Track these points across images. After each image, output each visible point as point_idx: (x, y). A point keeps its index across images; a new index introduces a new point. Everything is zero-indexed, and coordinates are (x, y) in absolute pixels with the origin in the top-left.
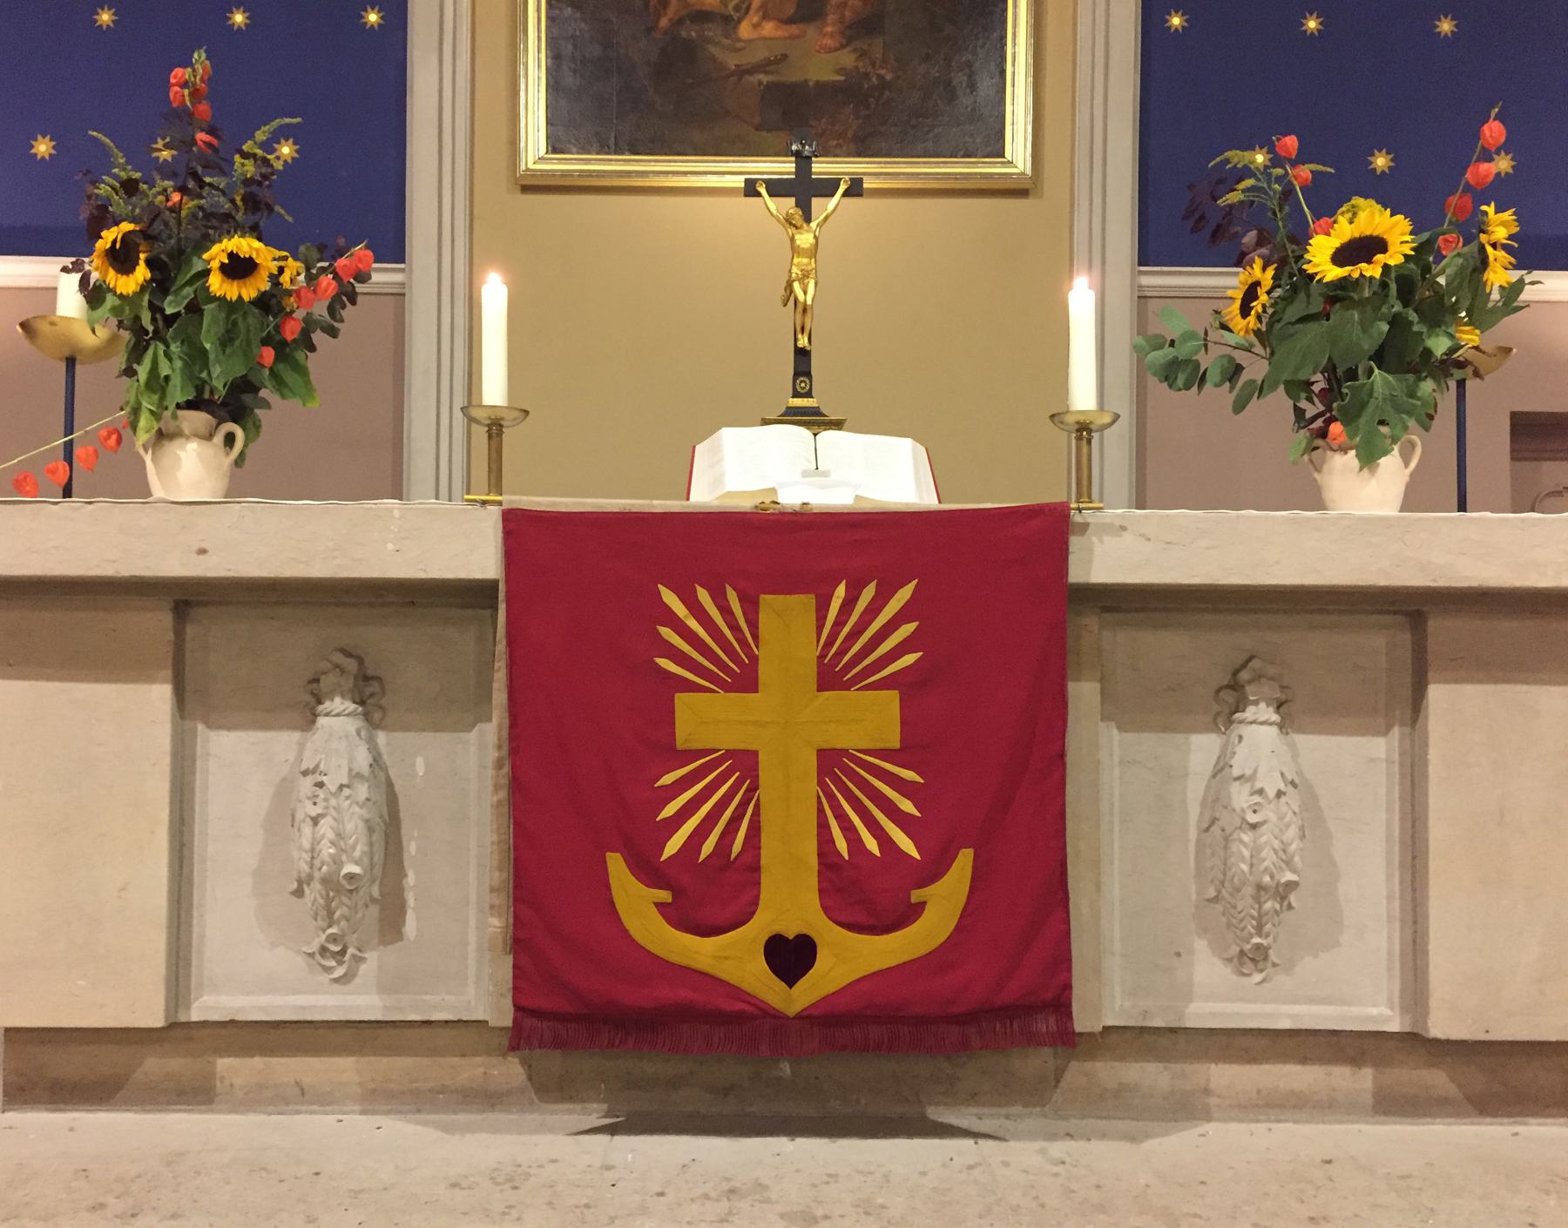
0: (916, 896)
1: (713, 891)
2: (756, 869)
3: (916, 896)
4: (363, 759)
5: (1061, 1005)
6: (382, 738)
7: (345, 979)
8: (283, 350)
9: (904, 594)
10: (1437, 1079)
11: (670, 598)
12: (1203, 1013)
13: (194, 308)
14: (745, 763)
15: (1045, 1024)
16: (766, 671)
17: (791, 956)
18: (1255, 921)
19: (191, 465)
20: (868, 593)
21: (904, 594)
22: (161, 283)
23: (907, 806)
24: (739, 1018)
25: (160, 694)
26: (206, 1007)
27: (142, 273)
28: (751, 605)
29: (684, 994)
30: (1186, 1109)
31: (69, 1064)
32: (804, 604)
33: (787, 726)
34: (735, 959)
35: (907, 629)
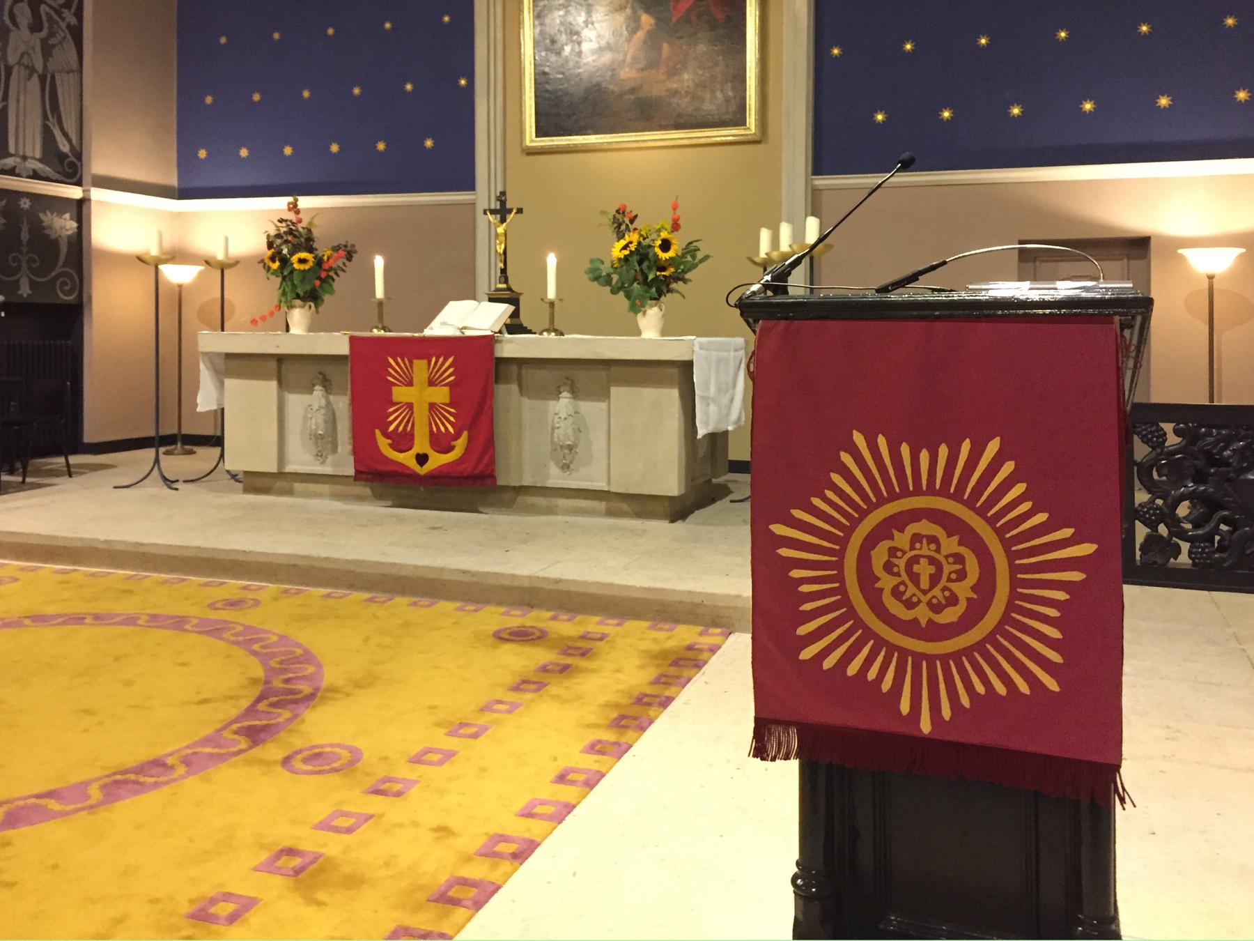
0: (453, 443)
1: (403, 441)
2: (413, 435)
3: (453, 443)
4: (323, 402)
5: (492, 477)
6: (331, 397)
7: (323, 463)
8: (323, 281)
9: (451, 360)
10: (625, 506)
11: (391, 361)
12: (551, 483)
13: (292, 272)
14: (410, 406)
15: (489, 482)
16: (415, 381)
17: (422, 459)
18: (567, 455)
19: (299, 317)
20: (441, 360)
21: (451, 360)
22: (282, 267)
23: (452, 419)
24: (407, 476)
25: (273, 384)
26: (289, 468)
27: (278, 263)
28: (411, 362)
29: (395, 468)
30: (550, 511)
31: (258, 482)
32: (424, 362)
33: (420, 394)
34: (407, 459)
35: (451, 370)
